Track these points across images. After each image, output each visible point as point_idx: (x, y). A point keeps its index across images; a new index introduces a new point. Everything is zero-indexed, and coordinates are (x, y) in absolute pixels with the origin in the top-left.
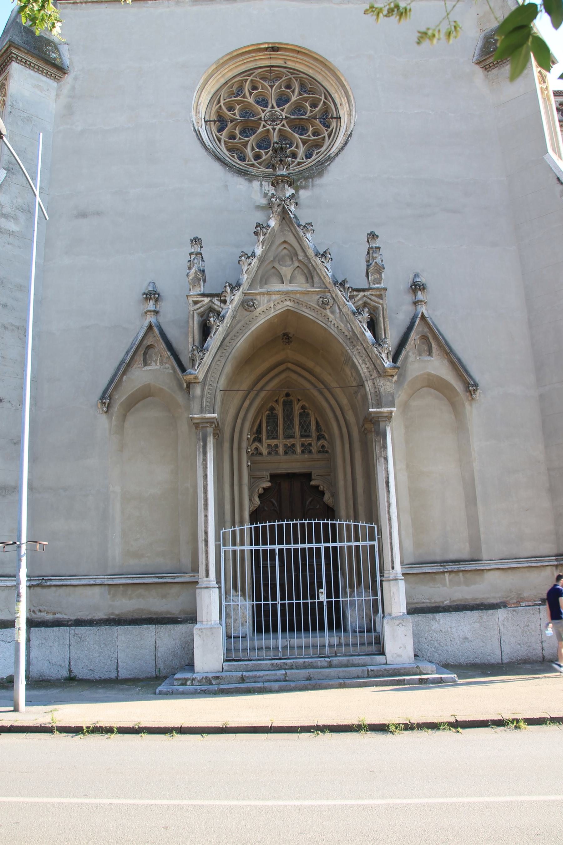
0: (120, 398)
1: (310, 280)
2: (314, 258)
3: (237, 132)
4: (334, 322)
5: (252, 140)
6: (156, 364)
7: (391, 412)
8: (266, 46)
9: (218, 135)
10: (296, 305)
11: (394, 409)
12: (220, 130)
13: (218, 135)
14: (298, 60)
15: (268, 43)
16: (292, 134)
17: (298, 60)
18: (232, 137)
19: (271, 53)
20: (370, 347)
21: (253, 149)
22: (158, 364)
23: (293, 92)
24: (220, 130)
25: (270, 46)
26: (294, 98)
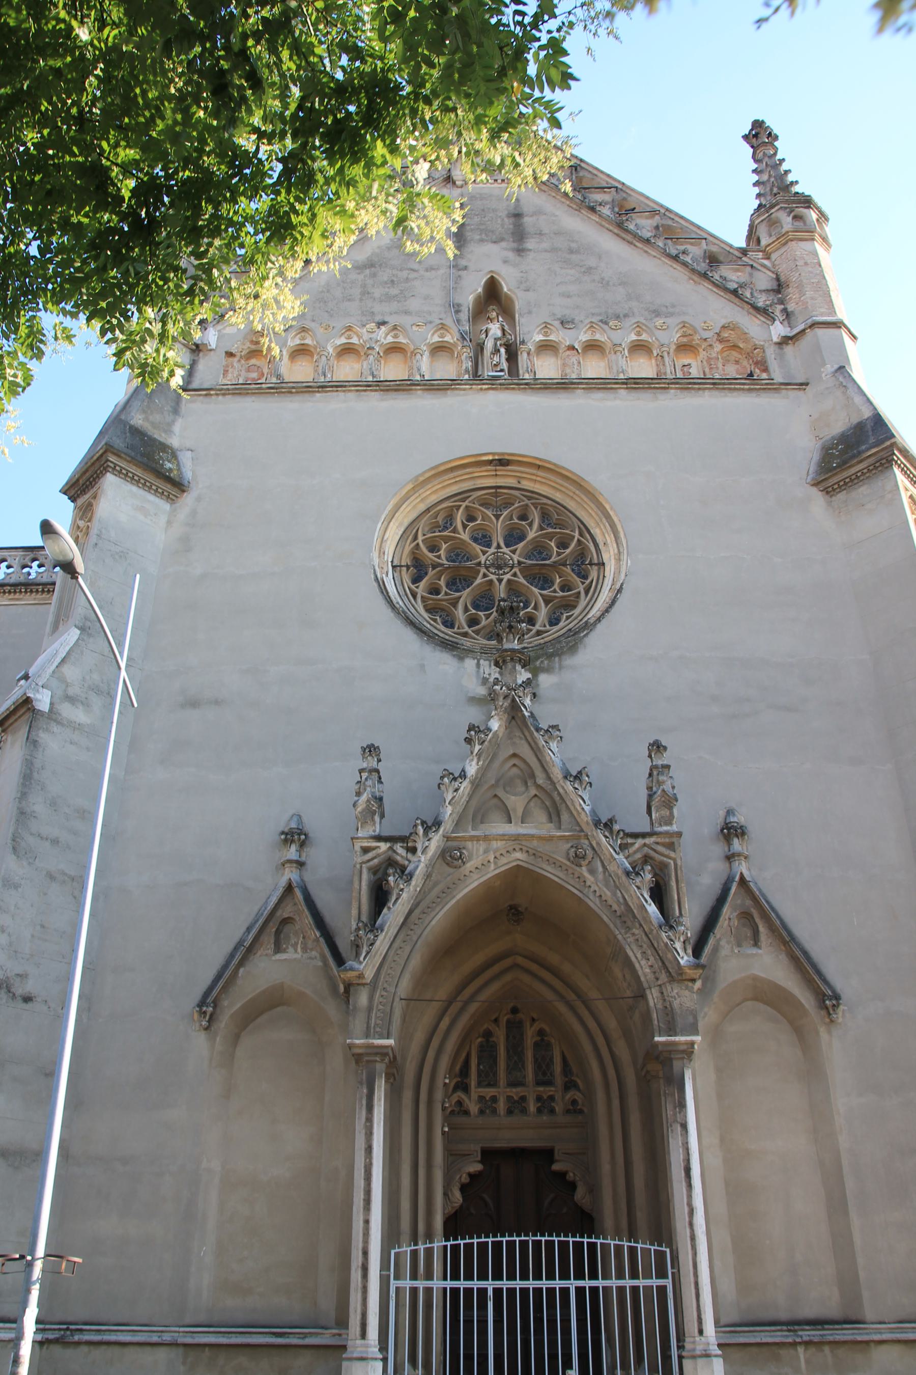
0: (232, 1005)
1: (555, 818)
2: (561, 782)
3: (442, 583)
4: (594, 887)
5: (466, 595)
6: (296, 951)
7: (692, 1044)
8: (491, 458)
9: (413, 587)
10: (531, 859)
11: (698, 1039)
12: (416, 580)
13: (413, 587)
14: (538, 479)
15: (493, 454)
16: (528, 588)
17: (538, 479)
18: (435, 590)
19: (498, 468)
20: (655, 932)
21: (466, 609)
22: (299, 950)
23: (531, 525)
24: (416, 580)
25: (497, 457)
26: (531, 535)
